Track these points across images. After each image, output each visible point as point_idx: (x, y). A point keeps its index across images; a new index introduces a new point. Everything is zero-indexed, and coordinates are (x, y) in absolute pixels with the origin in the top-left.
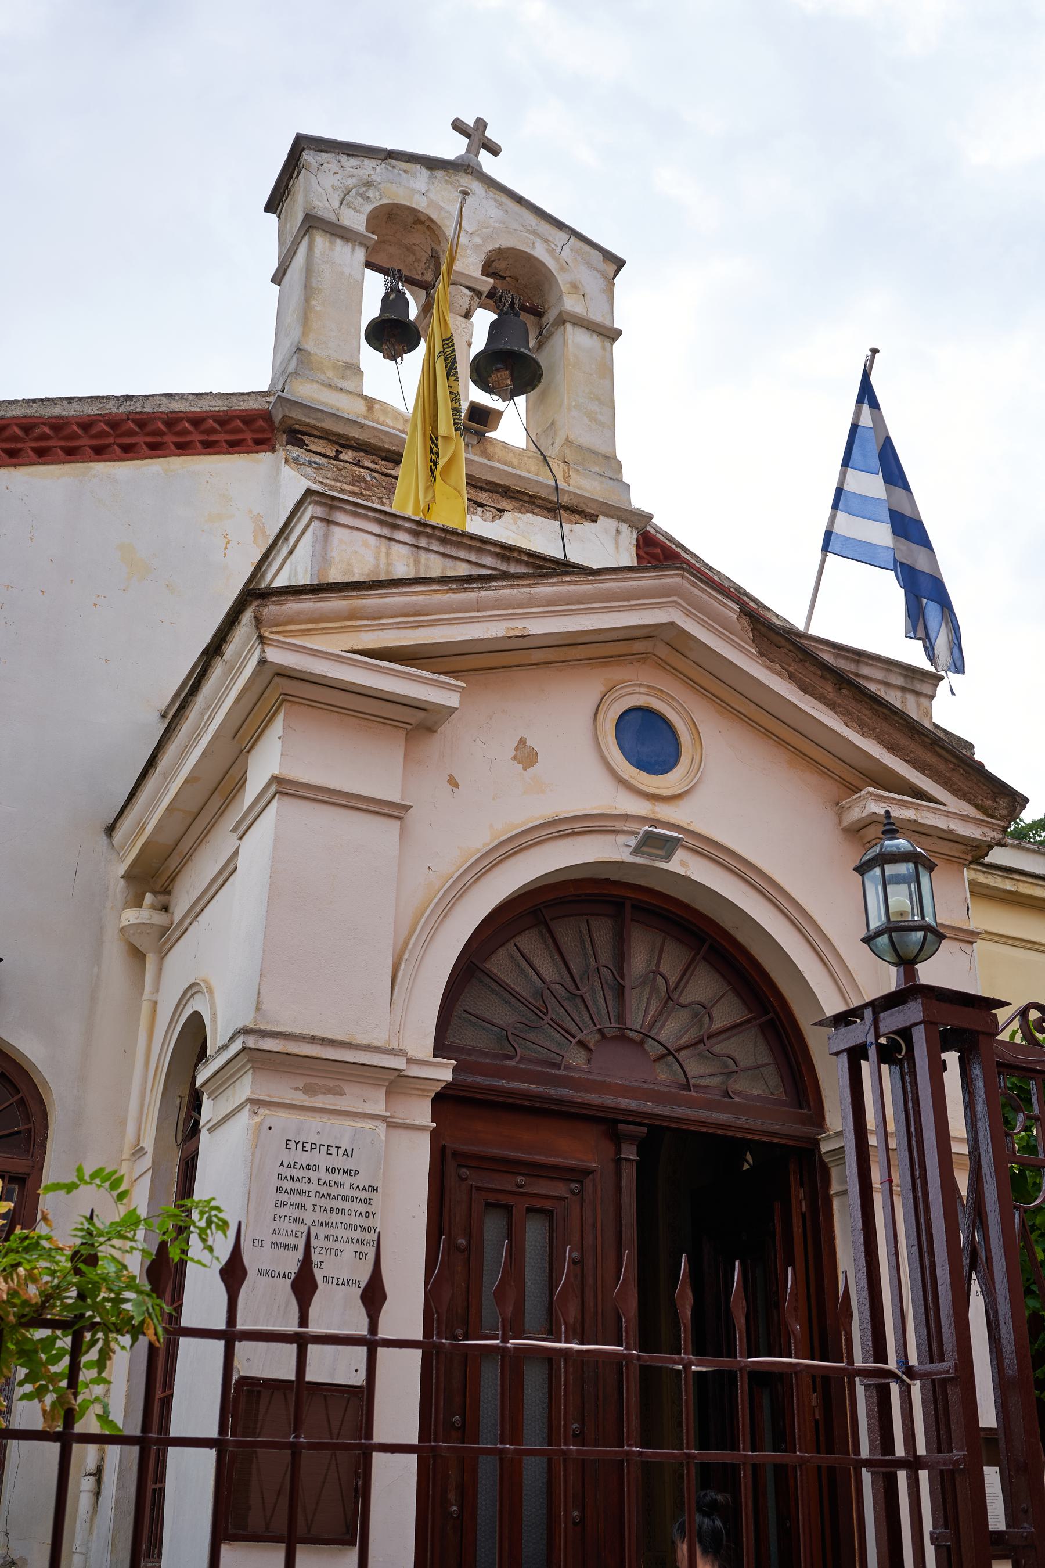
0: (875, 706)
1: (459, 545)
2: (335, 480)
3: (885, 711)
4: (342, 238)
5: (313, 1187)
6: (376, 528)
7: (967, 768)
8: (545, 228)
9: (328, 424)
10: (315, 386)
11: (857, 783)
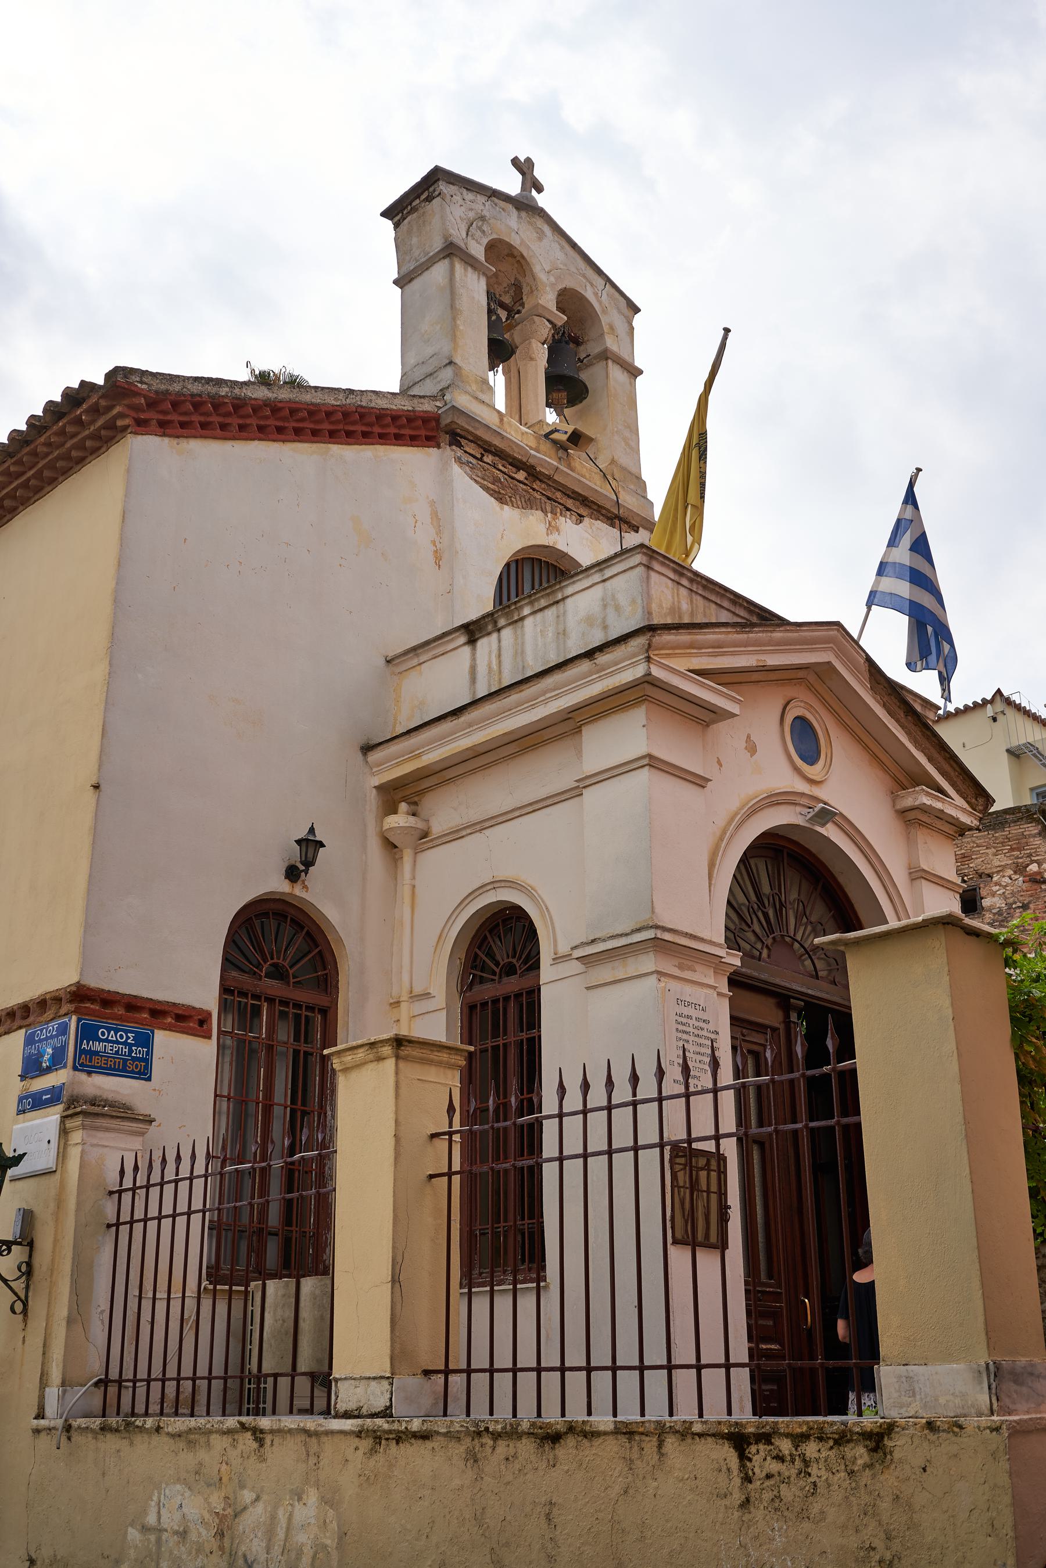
0: (924, 730)
1: (712, 591)
2: (483, 479)
3: (929, 733)
4: (472, 266)
5: (691, 1029)
6: (671, 575)
7: (965, 776)
8: (590, 272)
9: (480, 433)
10: (468, 397)
11: (906, 783)
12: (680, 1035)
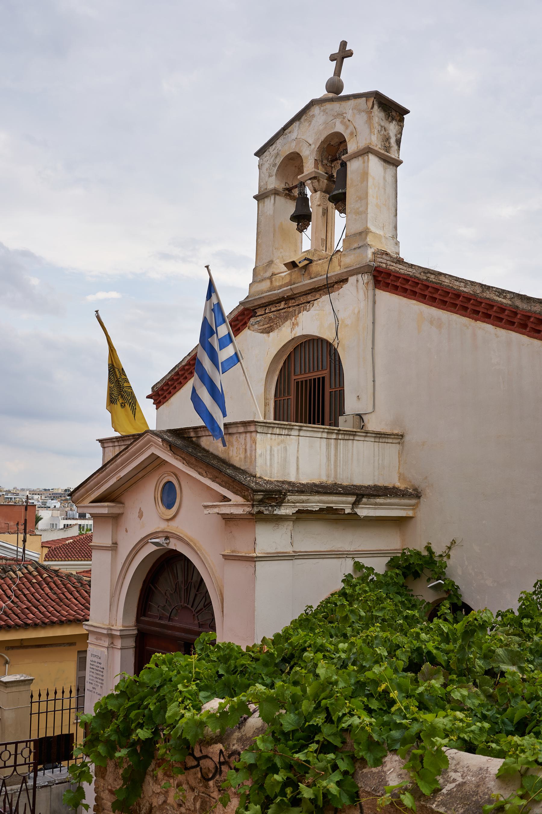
12: (91, 670)
